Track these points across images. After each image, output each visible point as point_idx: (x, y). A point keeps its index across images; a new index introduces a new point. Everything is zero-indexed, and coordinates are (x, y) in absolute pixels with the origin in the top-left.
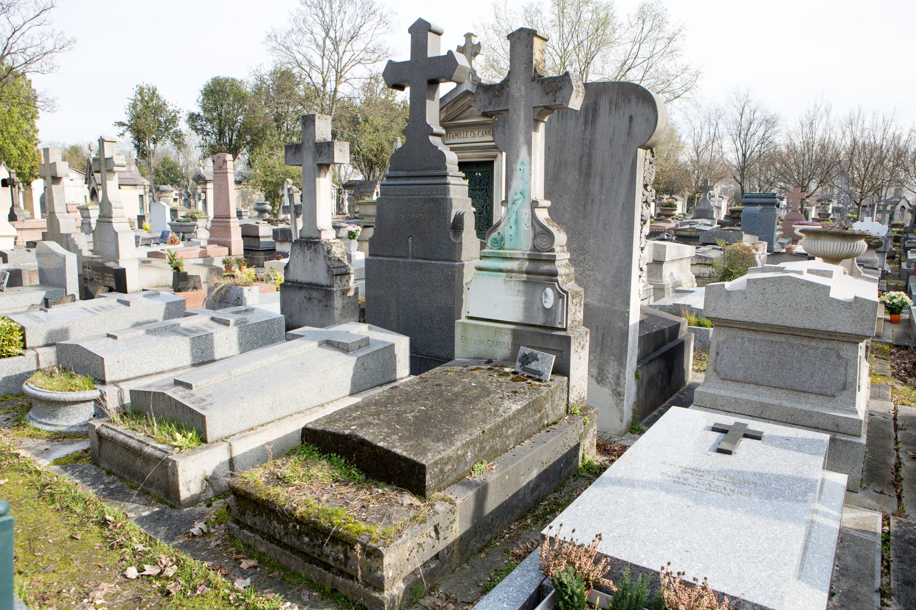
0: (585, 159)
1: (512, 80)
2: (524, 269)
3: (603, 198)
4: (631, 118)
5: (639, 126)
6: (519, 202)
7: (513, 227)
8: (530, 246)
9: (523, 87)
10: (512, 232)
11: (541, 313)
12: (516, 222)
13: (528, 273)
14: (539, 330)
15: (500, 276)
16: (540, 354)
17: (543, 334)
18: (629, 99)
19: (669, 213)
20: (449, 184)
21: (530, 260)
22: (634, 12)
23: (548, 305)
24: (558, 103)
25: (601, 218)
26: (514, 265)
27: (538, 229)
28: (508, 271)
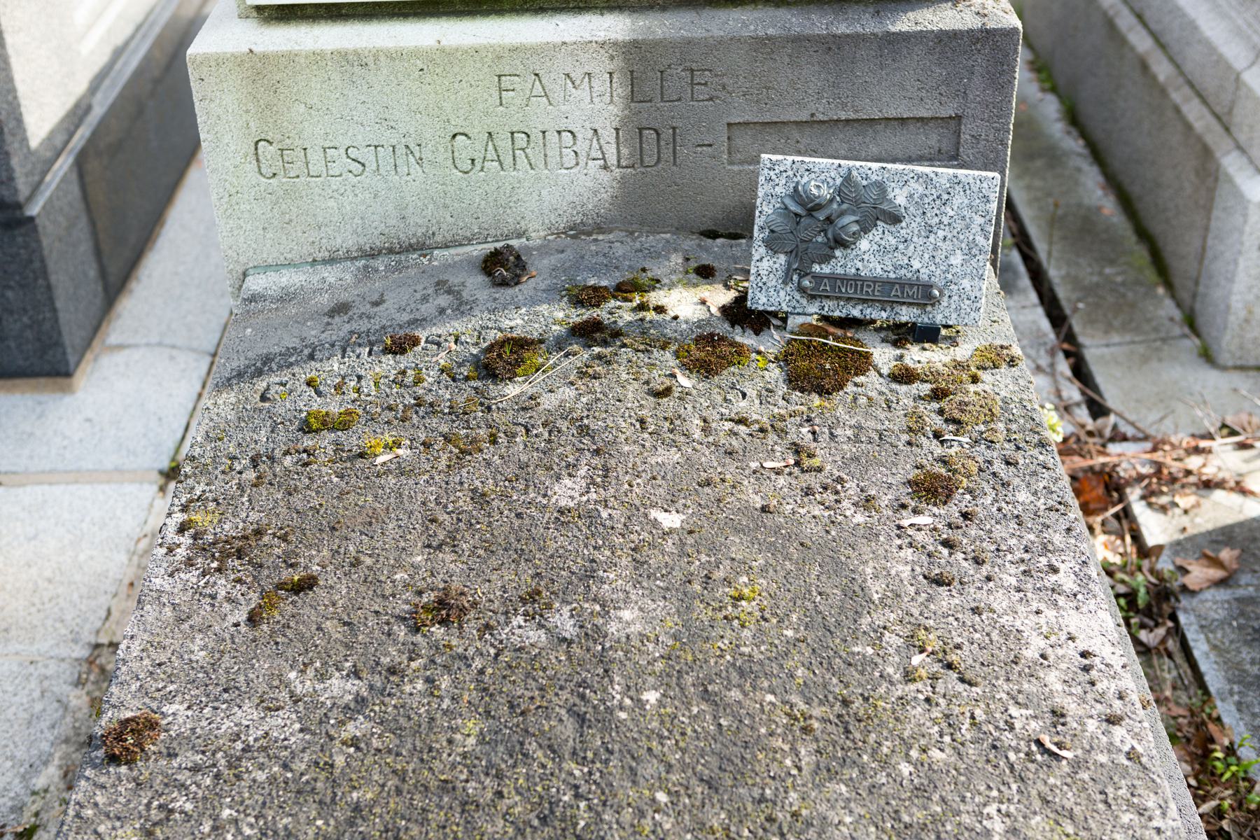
16: (904, 182)
17: (832, 45)
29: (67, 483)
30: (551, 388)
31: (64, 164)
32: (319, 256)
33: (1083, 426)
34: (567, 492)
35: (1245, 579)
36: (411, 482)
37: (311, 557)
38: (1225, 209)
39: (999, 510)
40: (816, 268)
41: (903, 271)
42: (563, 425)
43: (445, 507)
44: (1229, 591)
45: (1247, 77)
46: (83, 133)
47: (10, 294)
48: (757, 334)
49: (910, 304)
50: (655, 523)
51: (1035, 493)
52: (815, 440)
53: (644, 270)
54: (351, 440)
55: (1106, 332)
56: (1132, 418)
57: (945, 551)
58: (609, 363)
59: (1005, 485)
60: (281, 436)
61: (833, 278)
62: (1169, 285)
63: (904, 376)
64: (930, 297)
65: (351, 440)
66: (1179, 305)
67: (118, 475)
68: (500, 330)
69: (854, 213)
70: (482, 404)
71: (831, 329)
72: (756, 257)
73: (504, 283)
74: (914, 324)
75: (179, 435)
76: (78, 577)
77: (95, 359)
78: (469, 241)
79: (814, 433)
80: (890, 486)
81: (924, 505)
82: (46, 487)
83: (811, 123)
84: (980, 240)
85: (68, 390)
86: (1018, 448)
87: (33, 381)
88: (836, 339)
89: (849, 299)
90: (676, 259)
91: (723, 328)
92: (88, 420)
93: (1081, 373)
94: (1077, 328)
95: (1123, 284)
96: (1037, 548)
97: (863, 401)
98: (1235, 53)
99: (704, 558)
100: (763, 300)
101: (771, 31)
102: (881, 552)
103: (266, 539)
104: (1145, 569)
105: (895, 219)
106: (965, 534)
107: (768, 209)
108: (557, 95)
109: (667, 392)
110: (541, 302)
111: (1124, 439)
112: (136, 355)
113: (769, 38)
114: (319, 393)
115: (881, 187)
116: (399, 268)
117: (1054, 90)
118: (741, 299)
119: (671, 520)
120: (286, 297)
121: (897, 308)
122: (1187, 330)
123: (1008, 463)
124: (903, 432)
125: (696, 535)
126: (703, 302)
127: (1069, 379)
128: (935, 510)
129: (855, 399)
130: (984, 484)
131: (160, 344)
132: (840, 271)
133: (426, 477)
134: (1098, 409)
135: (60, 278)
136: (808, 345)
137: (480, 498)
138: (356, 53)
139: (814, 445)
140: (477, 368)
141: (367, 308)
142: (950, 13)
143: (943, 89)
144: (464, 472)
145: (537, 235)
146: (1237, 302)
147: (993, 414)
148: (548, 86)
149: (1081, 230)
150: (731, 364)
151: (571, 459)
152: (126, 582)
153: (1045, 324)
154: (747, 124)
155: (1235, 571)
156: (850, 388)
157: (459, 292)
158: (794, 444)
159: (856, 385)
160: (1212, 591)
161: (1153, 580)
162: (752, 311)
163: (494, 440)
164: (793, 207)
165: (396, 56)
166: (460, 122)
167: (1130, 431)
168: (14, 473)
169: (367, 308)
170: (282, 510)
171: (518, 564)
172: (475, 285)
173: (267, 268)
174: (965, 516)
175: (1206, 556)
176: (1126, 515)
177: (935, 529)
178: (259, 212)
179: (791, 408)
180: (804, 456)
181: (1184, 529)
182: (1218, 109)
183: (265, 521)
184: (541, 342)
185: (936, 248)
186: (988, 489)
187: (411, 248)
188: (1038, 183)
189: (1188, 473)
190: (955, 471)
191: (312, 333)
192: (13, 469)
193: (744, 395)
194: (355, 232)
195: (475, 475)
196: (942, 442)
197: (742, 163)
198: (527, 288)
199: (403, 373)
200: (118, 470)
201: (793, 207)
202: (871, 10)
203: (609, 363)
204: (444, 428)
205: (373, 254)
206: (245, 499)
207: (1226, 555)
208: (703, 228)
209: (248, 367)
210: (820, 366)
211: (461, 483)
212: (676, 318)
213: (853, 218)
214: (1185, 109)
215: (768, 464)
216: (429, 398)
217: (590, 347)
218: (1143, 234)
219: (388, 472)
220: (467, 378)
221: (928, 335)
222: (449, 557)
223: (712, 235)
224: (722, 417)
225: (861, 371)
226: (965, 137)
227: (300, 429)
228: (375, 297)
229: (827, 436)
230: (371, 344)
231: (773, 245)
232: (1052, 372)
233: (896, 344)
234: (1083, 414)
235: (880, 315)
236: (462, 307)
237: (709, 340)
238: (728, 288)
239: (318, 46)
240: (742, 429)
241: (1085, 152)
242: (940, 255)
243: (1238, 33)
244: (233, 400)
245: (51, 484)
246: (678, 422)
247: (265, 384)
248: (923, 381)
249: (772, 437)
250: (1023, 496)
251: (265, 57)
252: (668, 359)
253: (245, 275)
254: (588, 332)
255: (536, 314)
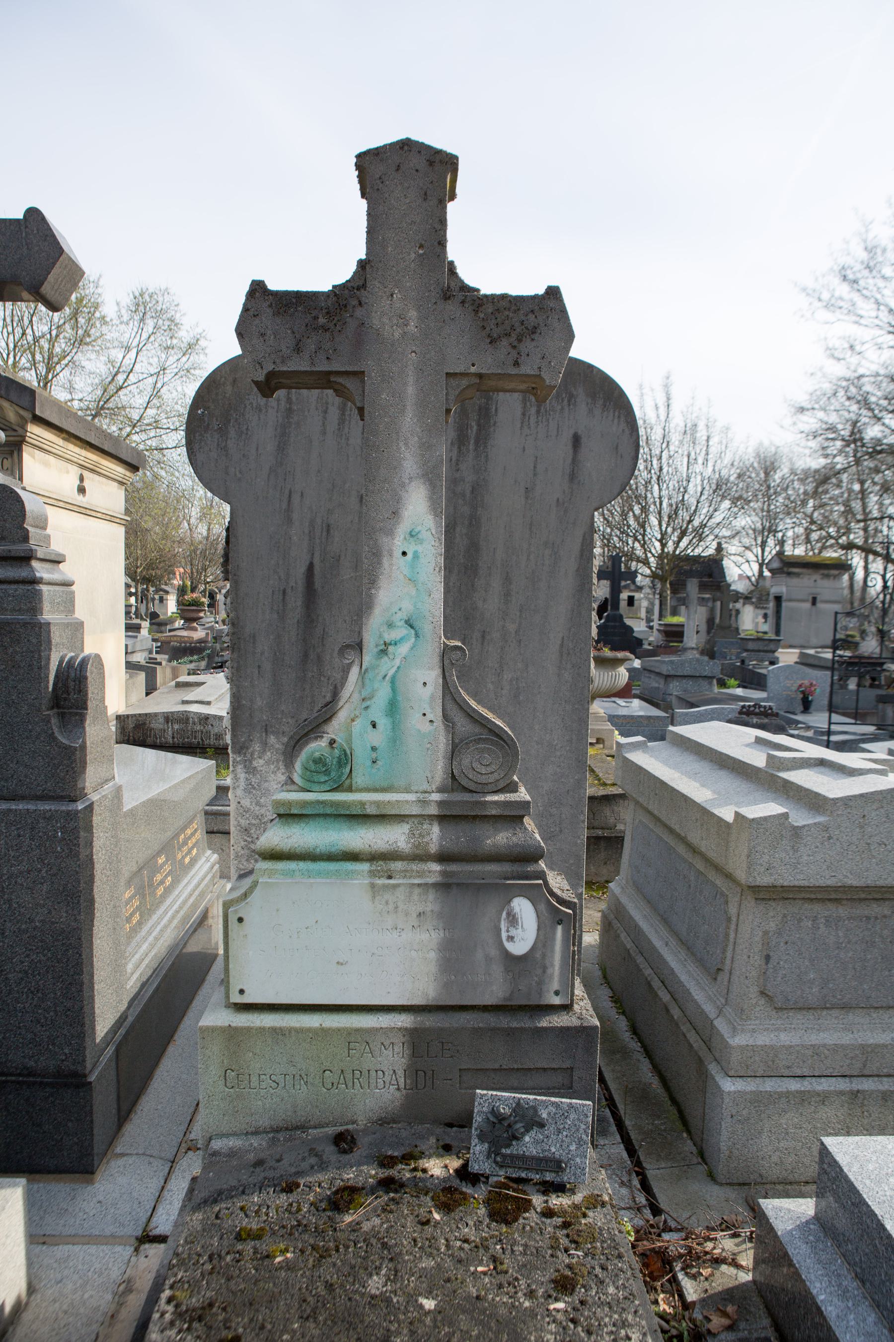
0: (461, 530)
1: (374, 285)
2: (433, 848)
3: (512, 627)
4: (576, 441)
5: (596, 461)
6: (403, 649)
7: (383, 722)
8: (439, 774)
9: (413, 314)
10: (378, 738)
11: (498, 971)
12: (393, 708)
13: (443, 858)
14: (492, 1020)
15: (349, 874)
16: (548, 1104)
17: (510, 1032)
18: (571, 397)
19: (194, 615)
20: (39, 581)
21: (442, 819)
22: (127, 300)
23: (519, 948)
24: (527, 369)
25: (507, 676)
26: (396, 837)
27: (464, 726)
28: (374, 857)
29: (84, 1244)
30: (366, 1217)
31: (110, 1050)
32: (250, 1130)
33: (648, 1221)
34: (375, 1284)
35: (742, 1325)
36: (293, 1275)
37: (238, 1324)
38: (712, 1093)
39: (599, 1298)
40: (503, 1151)
41: (546, 1153)
42: (374, 1241)
43: (311, 1292)
44: (734, 1334)
45: (715, 1023)
46: (122, 1031)
47: (70, 1124)
48: (474, 1186)
49: (551, 1171)
50: (421, 1306)
51: (617, 1288)
52: (504, 1253)
53: (416, 1146)
54: (264, 1246)
55: (657, 1161)
56: (675, 1215)
57: (572, 1326)
58: (398, 1203)
59: (602, 1282)
60: (225, 1243)
61: (512, 1156)
62: (689, 1132)
63: (548, 1213)
64: (560, 1167)
65: (264, 1246)
66: (695, 1145)
67: (112, 1239)
68: (342, 1180)
69: (521, 1122)
70: (332, 1226)
71: (511, 1184)
72: (473, 1144)
73: (345, 1152)
74: (553, 1182)
75: (149, 1214)
76: (82, 1310)
77: (108, 1163)
78: (327, 1125)
79: (503, 1249)
80: (542, 1284)
81: (560, 1295)
82: (70, 1246)
83: (500, 1070)
84: (584, 1136)
85: (91, 1182)
86: (608, 1259)
87: (72, 1176)
88: (514, 1191)
89: (520, 1168)
90: (432, 1140)
91: (456, 1183)
92: (100, 1202)
93: (646, 1187)
94: (642, 1158)
95: (665, 1130)
96: (619, 1323)
97: (528, 1228)
98: (709, 1009)
99: (447, 1329)
100: (477, 1167)
101: (481, 1025)
102: (539, 1326)
103: (215, 1310)
104: (686, 1318)
105: (542, 1125)
106: (582, 1315)
107: (479, 1119)
108: (377, 1053)
109: (427, 1222)
110: (363, 1164)
111: (671, 1230)
112: (130, 1160)
113: (480, 1028)
114: (247, 1216)
115: (535, 1109)
116: (291, 1139)
117: (624, 1013)
118: (465, 1166)
119: (429, 1304)
120: (232, 1154)
121: (544, 1173)
122: (700, 1160)
123: (603, 1269)
124: (548, 1248)
125: (442, 1314)
126: (446, 1167)
127: (639, 1190)
128: (566, 1298)
129: (524, 1228)
130: (591, 1282)
131: (144, 1154)
132: (515, 1152)
133: (301, 1272)
134: (656, 1211)
135: (98, 1118)
136: (499, 1194)
137: (329, 1287)
138: (280, 1028)
139: (503, 1256)
140: (330, 1203)
141: (273, 1163)
142: (566, 1017)
143: (564, 1054)
144: (322, 1269)
145: (362, 1122)
146: (723, 1146)
147: (594, 1238)
148: (373, 1048)
149: (641, 1096)
150: (460, 1205)
151: (377, 1264)
152: (110, 1314)
153: (625, 1155)
154: (469, 1069)
155: (736, 1320)
156: (521, 1221)
157: (321, 1156)
158: (493, 1256)
159: (524, 1218)
160: (725, 1333)
161: (691, 1326)
162: (471, 1174)
163: (337, 1250)
164: (492, 1119)
165: (299, 1031)
166: (328, 1064)
167: (673, 1224)
168: (54, 1236)
169: (273, 1163)
170: (224, 1290)
171: (349, 1331)
172: (329, 1150)
173: (222, 1136)
174: (582, 1303)
175: (721, 1310)
176: (674, 1280)
177: (566, 1311)
178: (222, 1106)
179: (492, 1233)
180: (498, 1263)
181: (707, 1290)
182: (704, 1037)
183: (214, 1298)
184: (363, 1188)
185: (562, 1141)
186: (593, 1286)
187: (297, 1128)
188: (618, 1068)
189: (706, 1253)
190: (576, 1274)
191: (244, 1177)
192: (54, 1233)
193: (467, 1225)
194: (270, 1118)
195: (327, 1272)
196: (569, 1255)
197: (466, 1088)
198: (357, 1154)
199: (291, 1205)
200: (113, 1236)
201: (492, 1119)
202: (528, 1015)
203: (398, 1203)
204: (312, 1241)
205: (277, 1130)
206: (205, 1282)
207: (730, 1309)
208: (446, 1121)
209: (210, 1197)
210: (505, 1210)
211: (320, 1277)
212: (432, 1176)
213: (521, 1125)
214: (688, 1035)
215: (480, 1269)
216: (305, 1222)
217: (388, 1193)
218: (674, 1101)
219: (281, 1268)
220: (324, 1210)
221: (560, 1188)
222: (312, 1325)
223: (451, 1125)
224: (456, 1239)
225: (526, 1210)
226: (575, 1078)
227: (236, 1238)
228: (278, 1157)
229: (509, 1251)
230: (275, 1186)
231: (482, 1138)
232: (630, 1186)
233: (545, 1193)
234: (647, 1212)
235: (537, 1177)
236: (323, 1166)
237: (449, 1190)
238: (459, 1158)
239: (263, 1025)
240: (466, 1245)
241: (642, 1050)
242: (565, 1145)
243: (710, 998)
244: (201, 1217)
245: (73, 1244)
246: (433, 1241)
247: (218, 1208)
248: (559, 1217)
249: (481, 1251)
250: (611, 1290)
251: (236, 1029)
252: (427, 1200)
253: (210, 1139)
254: (387, 1184)
255: (361, 1171)
